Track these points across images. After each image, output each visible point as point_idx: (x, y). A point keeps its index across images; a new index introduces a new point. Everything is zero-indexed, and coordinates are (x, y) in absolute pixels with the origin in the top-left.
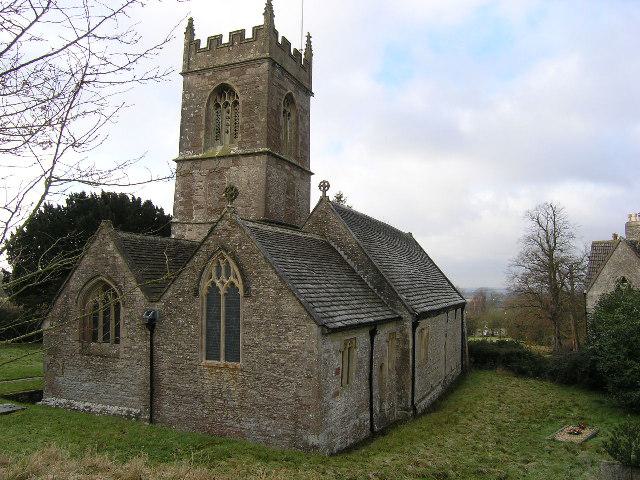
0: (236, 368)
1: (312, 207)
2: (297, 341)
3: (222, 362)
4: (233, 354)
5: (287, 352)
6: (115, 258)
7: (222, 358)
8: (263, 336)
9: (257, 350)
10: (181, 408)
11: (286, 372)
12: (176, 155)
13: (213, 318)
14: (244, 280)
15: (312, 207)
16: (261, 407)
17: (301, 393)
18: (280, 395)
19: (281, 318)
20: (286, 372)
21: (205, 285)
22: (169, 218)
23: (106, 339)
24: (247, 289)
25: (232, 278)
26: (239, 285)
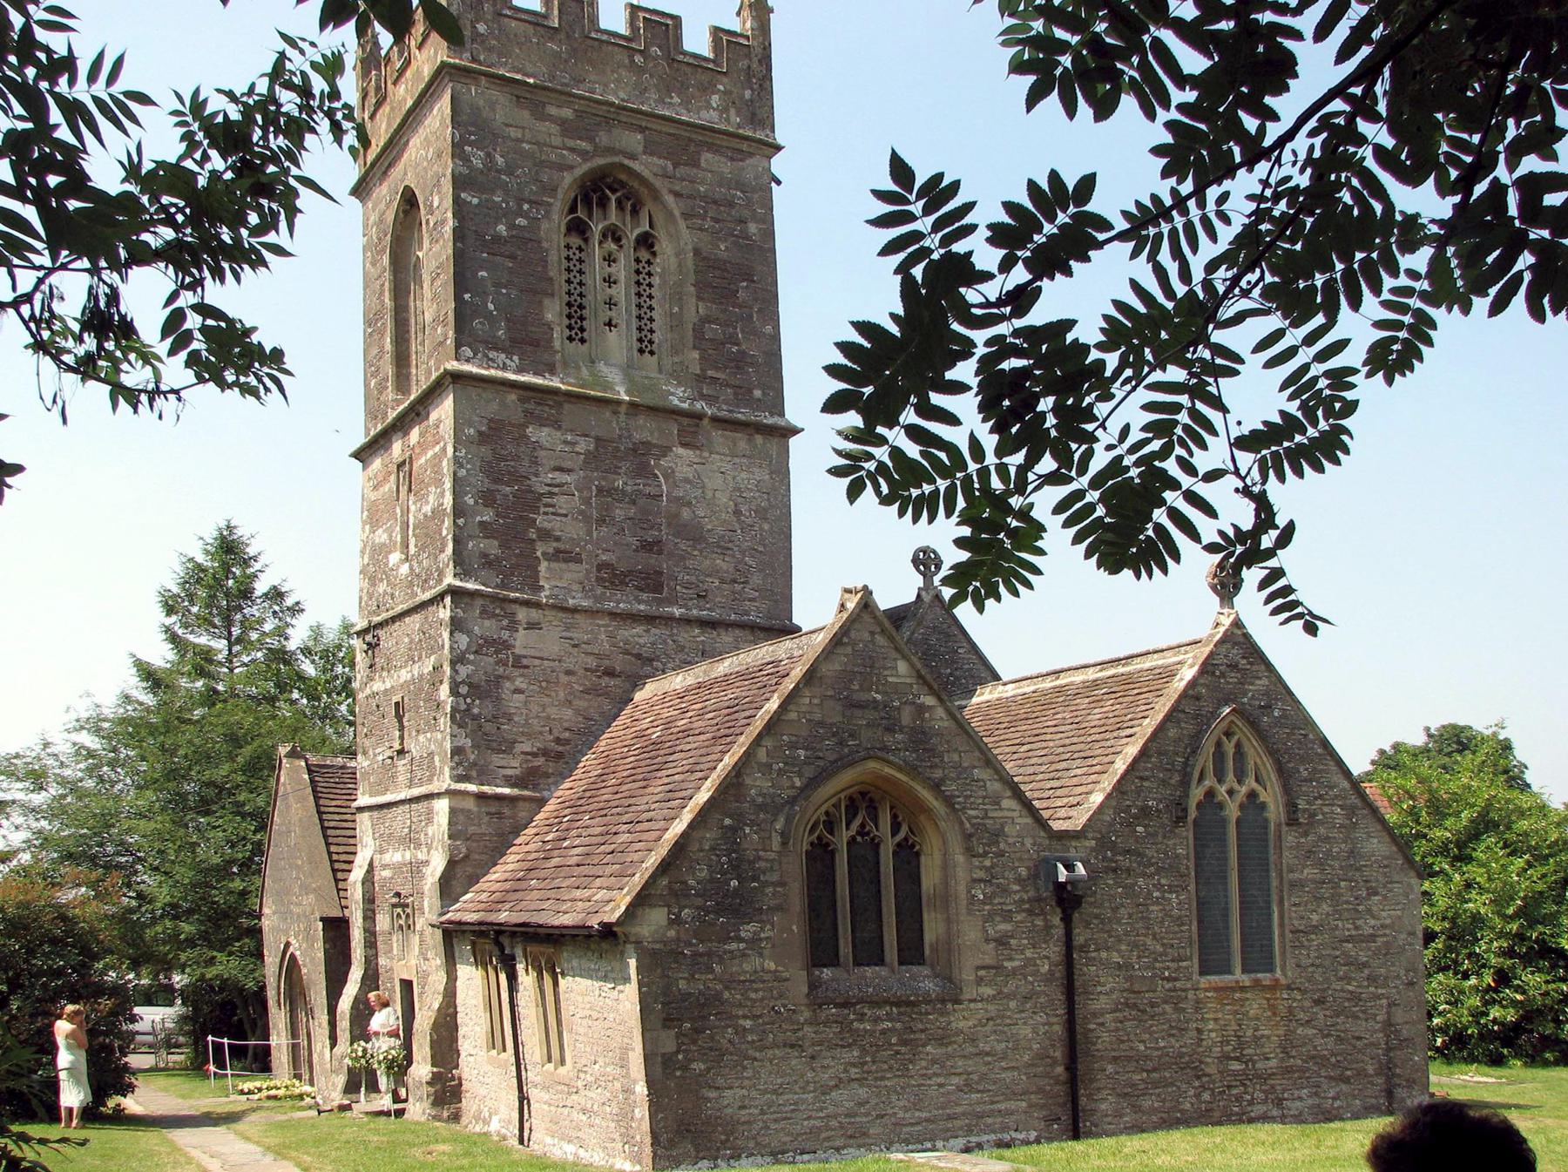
0: (1275, 986)
1: (1240, 113)
2: (1386, 916)
3: (1238, 976)
4: (1259, 956)
5: (1372, 938)
6: (922, 709)
7: (1238, 970)
8: (1325, 908)
9: (1316, 940)
10: (1146, 1103)
11: (1372, 979)
12: (778, 164)
13: (1208, 874)
14: (1287, 790)
15: (1240, 113)
16: (1322, 1061)
17: (1399, 1016)
18: (1360, 1028)
19: (1358, 869)
20: (1372, 979)
21: (1197, 794)
22: (177, 238)
23: (870, 953)
24: (1292, 808)
25: (1251, 783)
26: (1272, 798)
